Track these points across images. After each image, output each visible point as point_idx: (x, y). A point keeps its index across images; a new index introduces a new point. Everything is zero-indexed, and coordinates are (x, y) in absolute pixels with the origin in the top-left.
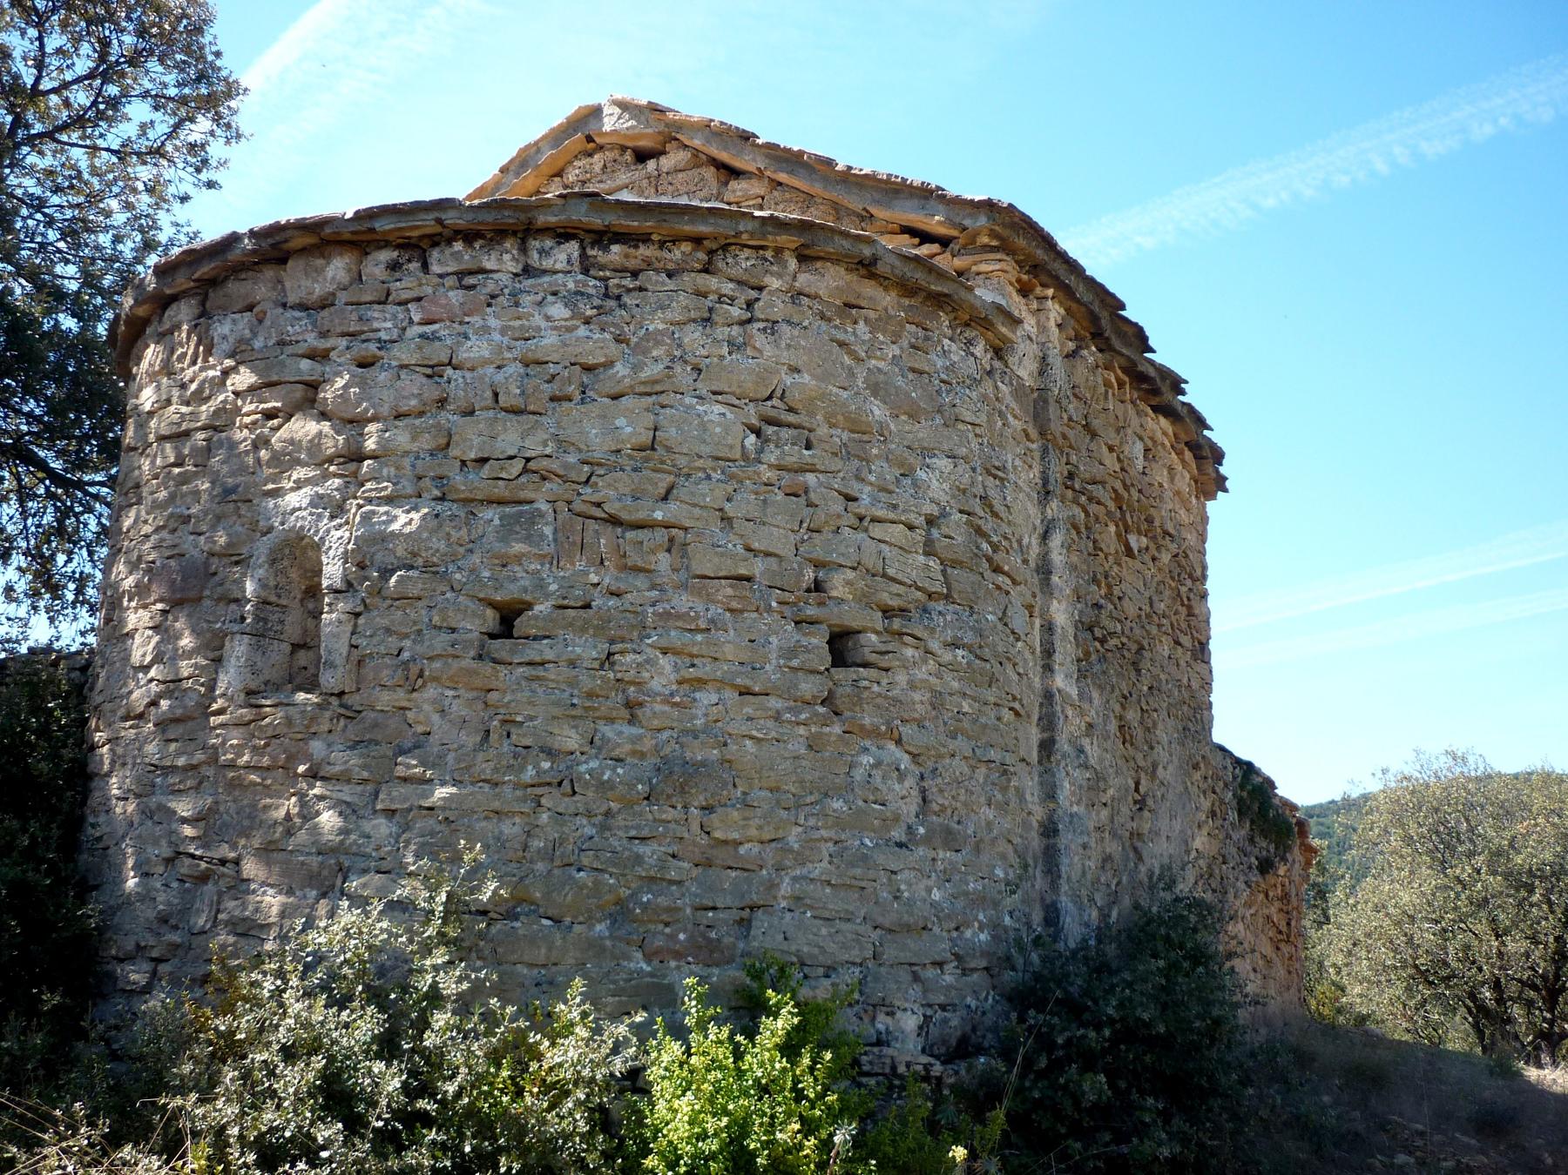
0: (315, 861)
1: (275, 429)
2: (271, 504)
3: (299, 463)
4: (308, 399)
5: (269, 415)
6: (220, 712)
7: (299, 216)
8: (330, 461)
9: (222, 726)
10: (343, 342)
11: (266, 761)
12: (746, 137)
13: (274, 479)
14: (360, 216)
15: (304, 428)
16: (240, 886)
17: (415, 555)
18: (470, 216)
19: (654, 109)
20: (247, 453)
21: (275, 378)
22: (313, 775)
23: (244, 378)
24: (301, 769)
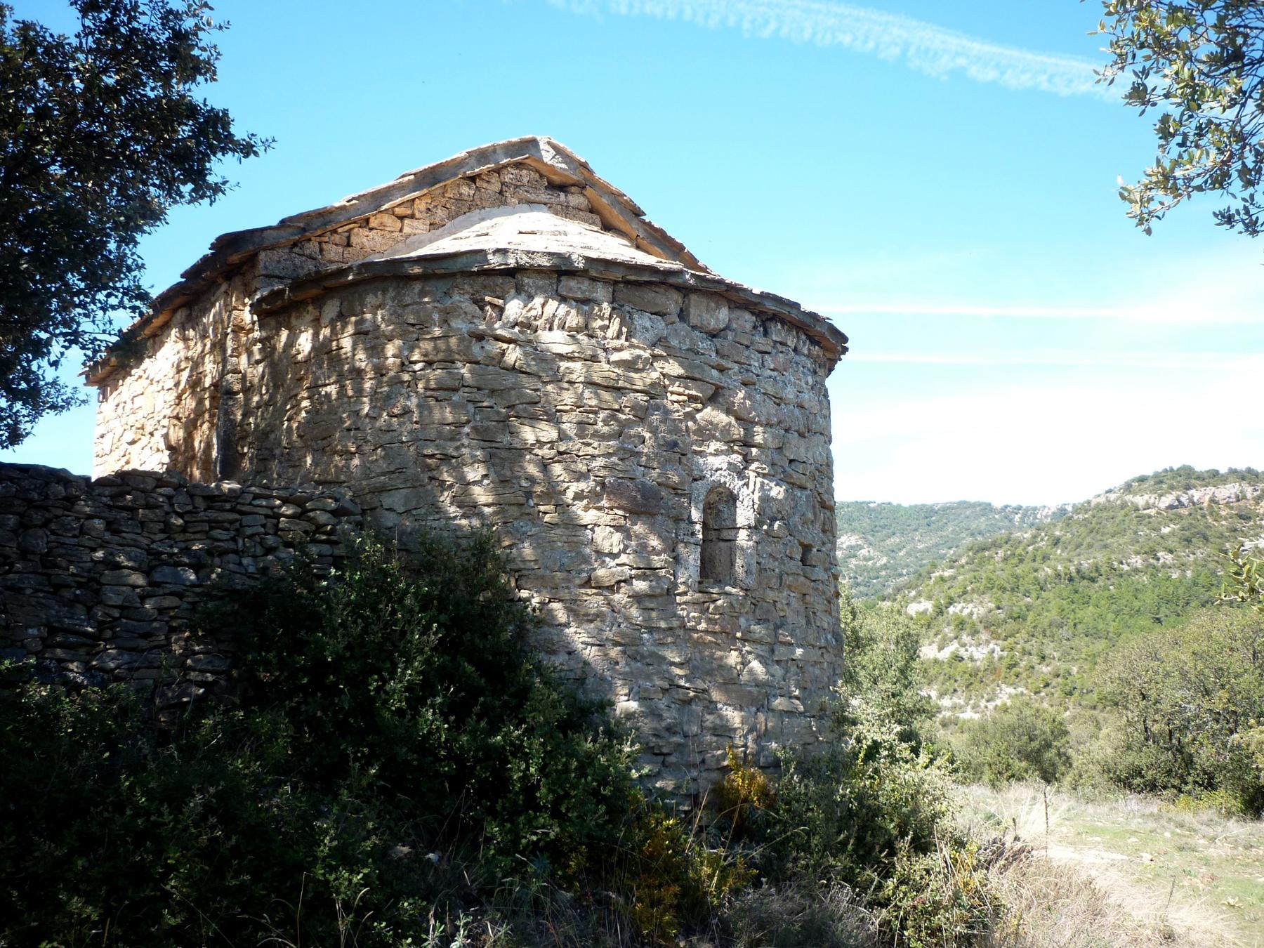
0: (755, 690)
1: (698, 411)
2: (701, 461)
3: (714, 437)
4: (715, 397)
5: (692, 399)
6: (685, 593)
7: (822, 312)
8: (734, 441)
9: (685, 603)
10: (736, 367)
11: (717, 628)
12: (637, 213)
13: (701, 443)
14: (764, 296)
15: (709, 414)
16: (711, 707)
17: (779, 512)
18: (801, 317)
19: (584, 166)
20: (681, 421)
21: (697, 376)
22: (744, 640)
23: (674, 368)
24: (739, 635)
